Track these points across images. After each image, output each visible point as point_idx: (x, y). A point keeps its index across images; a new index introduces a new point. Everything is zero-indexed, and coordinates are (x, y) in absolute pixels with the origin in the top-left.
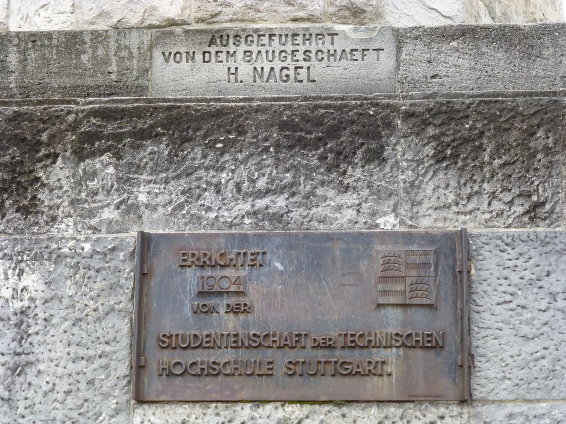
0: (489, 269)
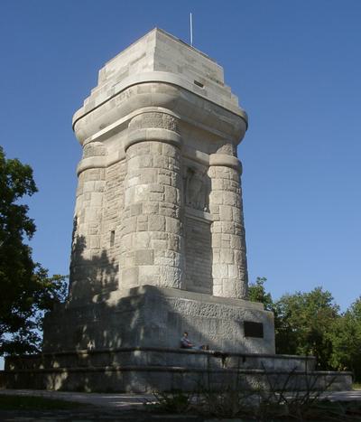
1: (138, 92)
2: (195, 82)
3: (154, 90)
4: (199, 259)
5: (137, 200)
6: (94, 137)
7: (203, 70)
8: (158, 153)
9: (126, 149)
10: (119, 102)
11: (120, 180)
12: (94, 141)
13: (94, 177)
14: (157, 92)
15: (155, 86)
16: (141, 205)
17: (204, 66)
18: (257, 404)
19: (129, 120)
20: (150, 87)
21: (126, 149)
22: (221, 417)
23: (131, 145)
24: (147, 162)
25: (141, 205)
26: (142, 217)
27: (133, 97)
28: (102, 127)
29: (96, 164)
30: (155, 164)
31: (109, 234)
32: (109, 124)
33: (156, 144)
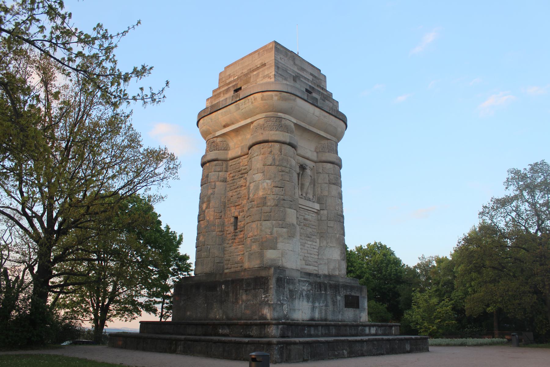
0: (360, 299)
1: (262, 99)
2: (307, 90)
3: (275, 98)
4: (309, 243)
5: (261, 193)
6: (218, 134)
7: (310, 78)
8: (279, 153)
9: (250, 148)
10: (244, 106)
11: (243, 173)
12: (217, 137)
13: (218, 168)
14: (278, 100)
15: (276, 95)
16: (265, 198)
17: (312, 74)
18: (215, 306)
19: (252, 123)
20: (272, 96)
21: (250, 148)
22: (316, 352)
23: (254, 145)
24: (270, 161)
25: (265, 198)
26: (266, 209)
27: (256, 104)
28: (225, 126)
29: (220, 157)
30: (277, 163)
31: (232, 220)
32: (233, 124)
33: (277, 145)
